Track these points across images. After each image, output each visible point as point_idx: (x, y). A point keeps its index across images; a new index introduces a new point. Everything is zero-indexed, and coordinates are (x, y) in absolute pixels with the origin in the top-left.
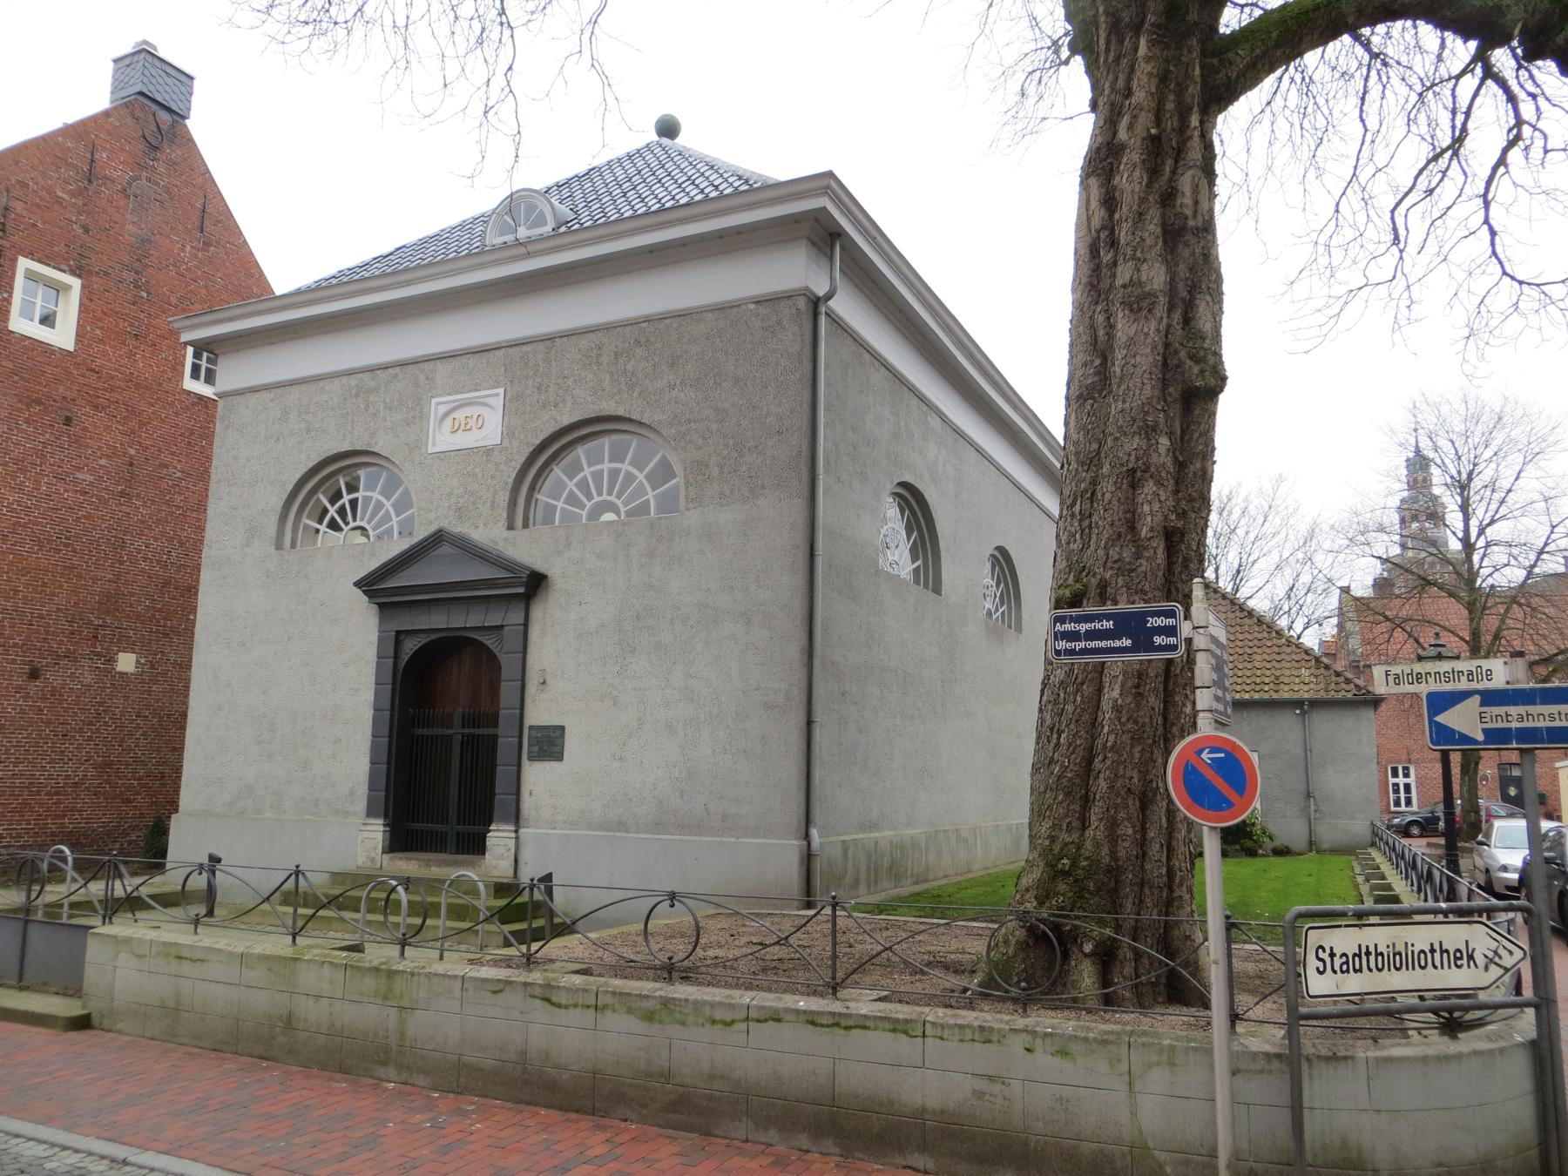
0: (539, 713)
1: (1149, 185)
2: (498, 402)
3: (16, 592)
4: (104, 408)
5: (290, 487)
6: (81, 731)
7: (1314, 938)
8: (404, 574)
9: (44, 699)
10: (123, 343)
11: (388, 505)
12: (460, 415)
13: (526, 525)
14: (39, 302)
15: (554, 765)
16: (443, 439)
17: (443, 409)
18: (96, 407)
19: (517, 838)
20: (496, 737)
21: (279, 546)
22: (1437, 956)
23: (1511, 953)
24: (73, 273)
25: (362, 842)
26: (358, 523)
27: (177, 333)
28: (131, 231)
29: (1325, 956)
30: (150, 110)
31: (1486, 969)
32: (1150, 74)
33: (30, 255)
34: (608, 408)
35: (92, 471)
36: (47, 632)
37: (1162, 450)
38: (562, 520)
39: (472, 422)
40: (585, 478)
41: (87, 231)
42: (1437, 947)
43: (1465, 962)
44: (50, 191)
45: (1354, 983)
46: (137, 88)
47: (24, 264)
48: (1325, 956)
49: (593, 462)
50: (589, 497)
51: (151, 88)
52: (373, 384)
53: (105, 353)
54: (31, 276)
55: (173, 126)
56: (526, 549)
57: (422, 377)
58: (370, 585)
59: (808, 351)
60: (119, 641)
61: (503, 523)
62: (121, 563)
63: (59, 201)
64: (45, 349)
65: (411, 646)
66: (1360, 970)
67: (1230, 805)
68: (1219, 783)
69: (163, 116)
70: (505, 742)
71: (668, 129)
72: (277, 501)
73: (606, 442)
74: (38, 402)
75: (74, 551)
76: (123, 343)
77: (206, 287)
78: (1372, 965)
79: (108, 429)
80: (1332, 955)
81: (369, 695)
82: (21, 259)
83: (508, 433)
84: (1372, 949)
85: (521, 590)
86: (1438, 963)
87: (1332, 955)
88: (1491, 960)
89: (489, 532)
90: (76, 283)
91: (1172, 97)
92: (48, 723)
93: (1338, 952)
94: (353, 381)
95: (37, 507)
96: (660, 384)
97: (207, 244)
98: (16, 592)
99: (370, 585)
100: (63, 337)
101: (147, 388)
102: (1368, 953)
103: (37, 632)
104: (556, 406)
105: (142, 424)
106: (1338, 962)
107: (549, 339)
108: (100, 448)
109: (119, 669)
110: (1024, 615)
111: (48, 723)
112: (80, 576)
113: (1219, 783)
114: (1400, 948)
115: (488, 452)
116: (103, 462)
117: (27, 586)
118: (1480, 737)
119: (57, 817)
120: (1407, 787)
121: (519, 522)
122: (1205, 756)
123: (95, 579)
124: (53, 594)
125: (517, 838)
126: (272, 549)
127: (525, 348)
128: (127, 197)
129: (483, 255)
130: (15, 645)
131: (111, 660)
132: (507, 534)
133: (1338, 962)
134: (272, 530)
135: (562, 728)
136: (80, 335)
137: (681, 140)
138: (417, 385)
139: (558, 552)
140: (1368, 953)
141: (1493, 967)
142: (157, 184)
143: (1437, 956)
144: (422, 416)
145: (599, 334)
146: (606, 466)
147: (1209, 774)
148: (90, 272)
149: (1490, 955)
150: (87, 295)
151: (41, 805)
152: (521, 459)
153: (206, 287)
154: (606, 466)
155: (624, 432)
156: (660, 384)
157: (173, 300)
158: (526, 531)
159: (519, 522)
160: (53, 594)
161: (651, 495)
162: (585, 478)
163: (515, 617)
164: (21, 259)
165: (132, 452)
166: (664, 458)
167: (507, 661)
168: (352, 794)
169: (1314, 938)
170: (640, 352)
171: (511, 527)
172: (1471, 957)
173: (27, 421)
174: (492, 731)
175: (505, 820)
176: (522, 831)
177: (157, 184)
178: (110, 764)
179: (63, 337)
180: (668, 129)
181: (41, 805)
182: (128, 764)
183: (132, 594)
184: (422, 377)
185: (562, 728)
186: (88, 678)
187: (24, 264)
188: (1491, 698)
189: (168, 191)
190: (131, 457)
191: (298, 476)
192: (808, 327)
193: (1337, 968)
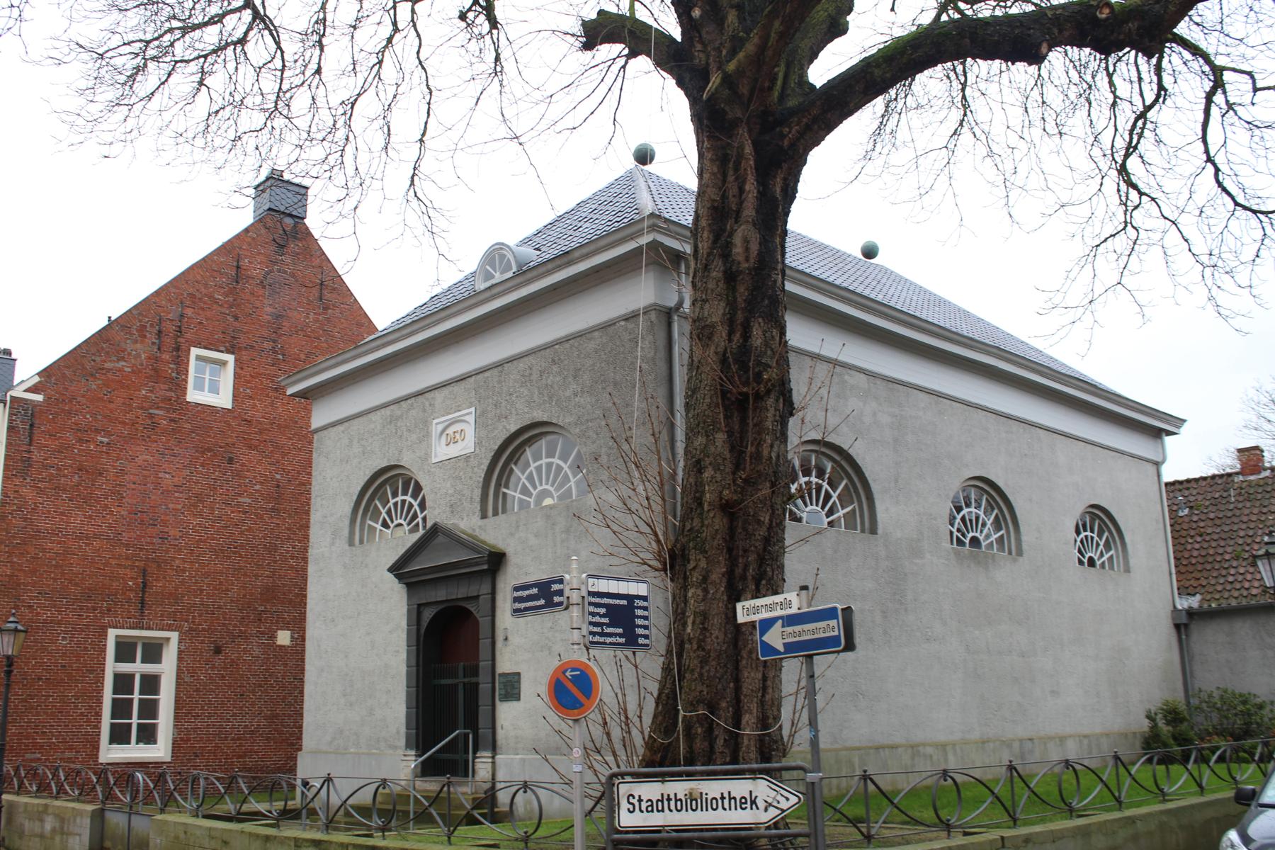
0: (505, 665)
1: (715, 242)
2: (471, 419)
3: (202, 591)
4: (256, 447)
5: (355, 498)
6: (253, 692)
7: (624, 789)
8: (418, 559)
9: (225, 668)
10: (267, 396)
12: (450, 431)
13: (495, 514)
14: (207, 377)
15: (515, 703)
16: (442, 451)
17: (440, 427)
18: (250, 448)
19: (493, 763)
20: (477, 684)
21: (351, 543)
22: (726, 802)
23: (787, 799)
24: (228, 352)
25: (401, 766)
26: (396, 522)
27: (284, 389)
28: (268, 310)
29: (635, 801)
30: (281, 220)
31: (766, 810)
32: (711, 160)
33: (199, 345)
34: (539, 415)
35: (250, 495)
36: (225, 619)
37: (719, 443)
38: (521, 508)
39: (458, 435)
41: (236, 318)
42: (726, 795)
43: (748, 805)
44: (211, 297)
45: (656, 820)
46: (266, 207)
47: (195, 352)
48: (635, 801)
49: (536, 461)
51: (277, 203)
52: (399, 413)
53: (254, 406)
54: (199, 358)
55: (295, 226)
56: (493, 533)
57: (427, 404)
58: (397, 569)
59: (662, 354)
60: (277, 622)
61: (478, 513)
62: (275, 562)
63: (216, 301)
64: (212, 410)
65: (428, 614)
66: (663, 810)
67: (582, 705)
68: (575, 691)
69: (288, 221)
70: (484, 687)
72: (347, 508)
73: (543, 443)
74: (209, 450)
75: (241, 556)
76: (267, 396)
77: (326, 341)
78: (673, 807)
79: (260, 463)
80: (640, 800)
81: (404, 656)
82: (192, 349)
83: (478, 443)
84: (672, 796)
85: (485, 567)
86: (726, 806)
87: (640, 800)
88: (770, 805)
89: (467, 522)
90: (230, 358)
91: (731, 172)
92: (230, 686)
93: (644, 798)
94: (387, 411)
95: (213, 527)
96: (568, 393)
97: (326, 308)
98: (202, 591)
99: (397, 569)
100: (223, 399)
101: (286, 427)
102: (669, 799)
103: (218, 619)
105: (284, 455)
106: (644, 805)
107: (499, 365)
108: (255, 477)
109: (279, 643)
110: (1024, 538)
111: (230, 686)
112: (245, 575)
113: (575, 691)
114: (696, 795)
115: (467, 458)
116: (258, 487)
117: (209, 585)
118: (782, 649)
119: (240, 757)
120: (151, 683)
121: (490, 512)
122: (568, 674)
123: (257, 576)
124: (228, 590)
125: (493, 763)
126: (346, 546)
127: (487, 374)
128: (264, 287)
129: (475, 298)
130: (204, 629)
131: (273, 637)
132: (481, 522)
133: (644, 805)
134: (346, 532)
135: (519, 674)
136: (235, 397)
138: (424, 411)
139: (512, 534)
140: (669, 799)
141: (771, 809)
142: (285, 272)
143: (726, 802)
144: (428, 435)
145: (531, 358)
146: (544, 461)
147: (570, 685)
148: (240, 349)
149: (770, 800)
150: (239, 364)
151: (229, 748)
152: (486, 462)
153: (326, 341)
156: (568, 393)
157: (303, 357)
158: (501, 517)
159: (490, 512)
160: (228, 590)
163: (485, 588)
164: (192, 349)
165: (278, 477)
166: (579, 452)
167: (484, 622)
168: (398, 732)
169: (624, 789)
170: (555, 369)
171: (484, 516)
172: (753, 802)
173: (203, 465)
174: (474, 680)
175: (485, 749)
176: (498, 757)
177: (285, 272)
178: (276, 716)
179: (223, 399)
181: (229, 748)
182: (290, 716)
183: (284, 585)
184: (427, 404)
185: (519, 674)
186: (257, 651)
187: (195, 352)
188: (791, 620)
189: (293, 275)
190: (278, 481)
192: (661, 335)
193: (644, 808)
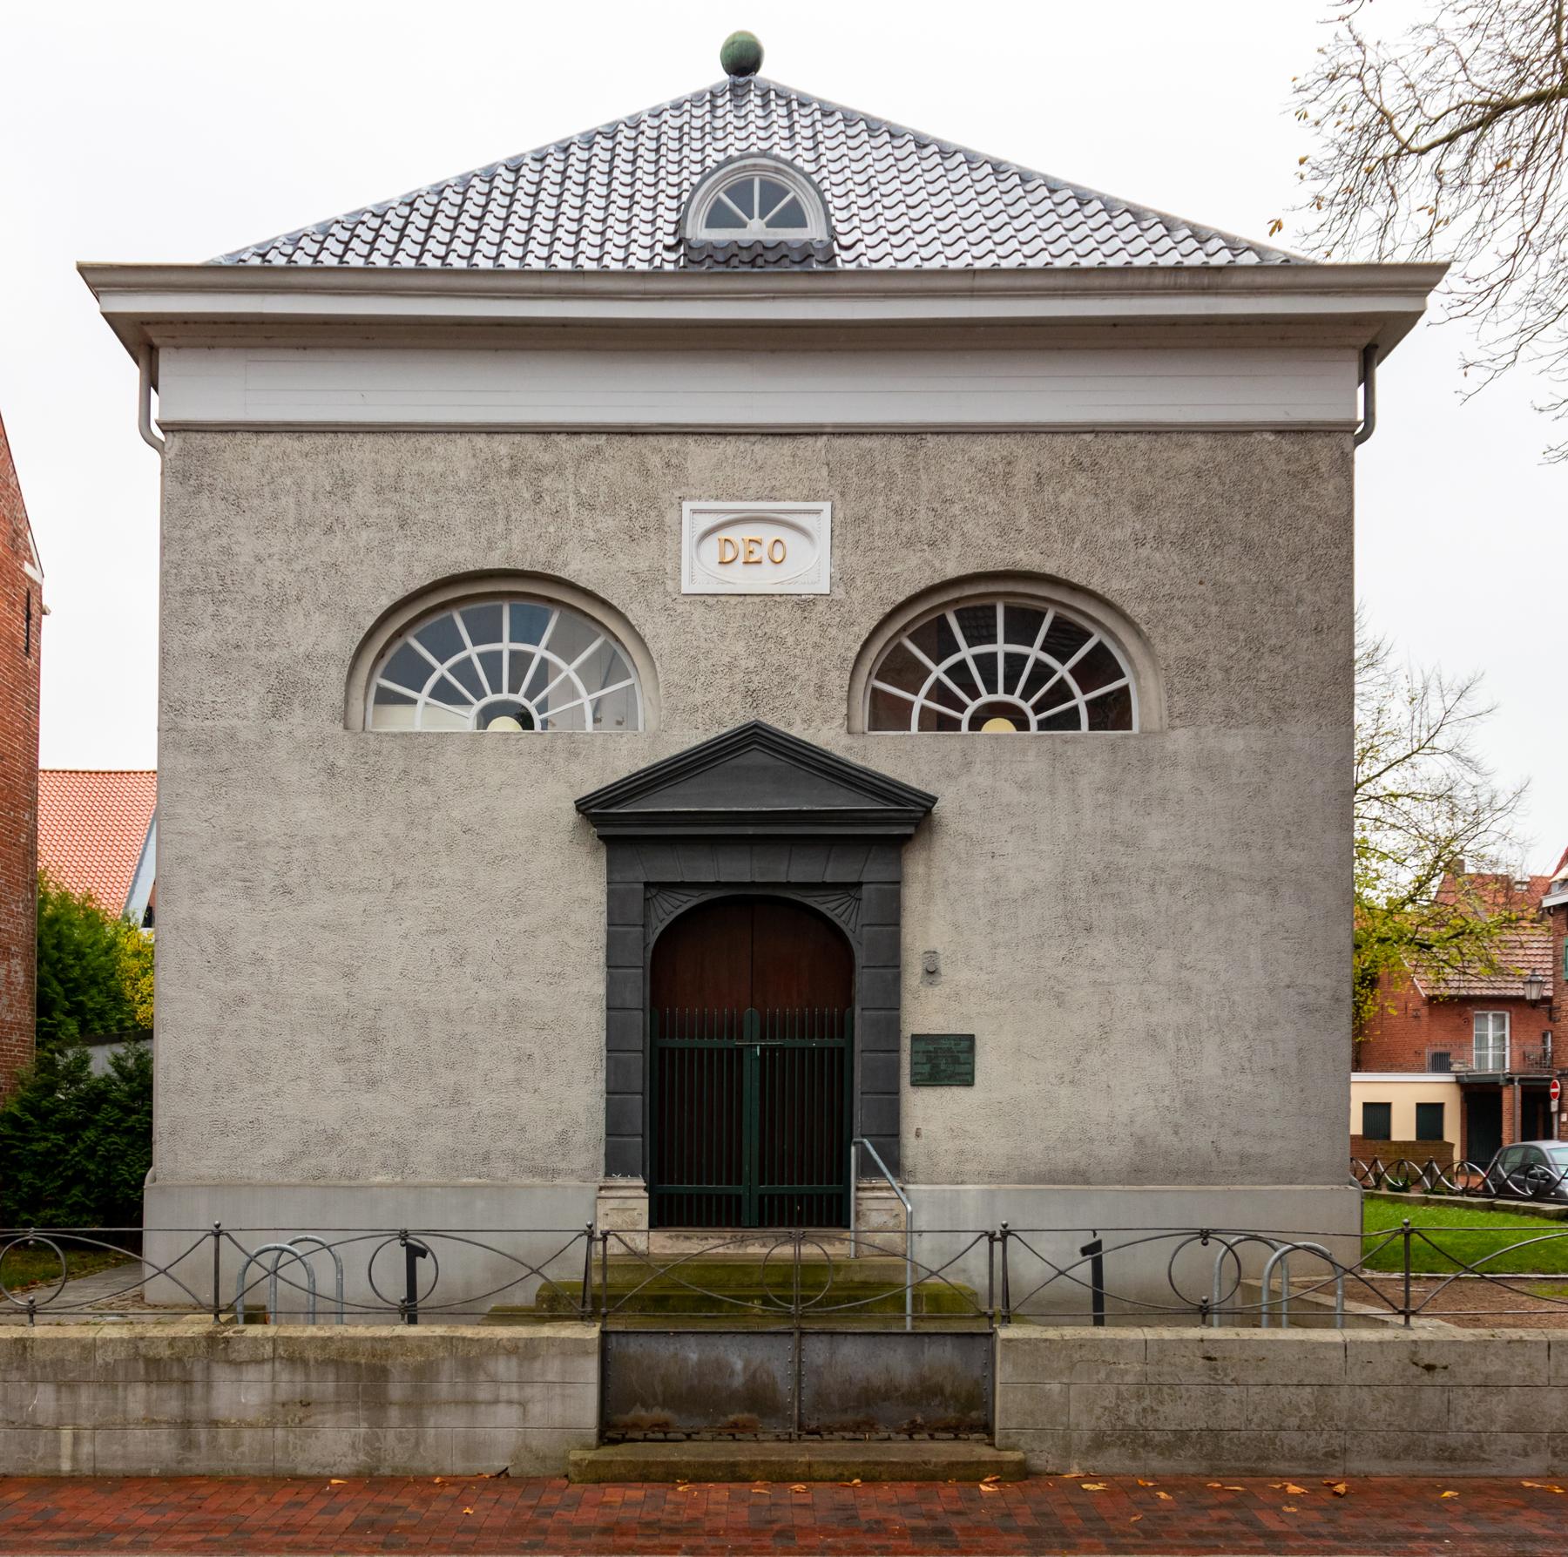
12: (738, 534)
104: (932, 544)
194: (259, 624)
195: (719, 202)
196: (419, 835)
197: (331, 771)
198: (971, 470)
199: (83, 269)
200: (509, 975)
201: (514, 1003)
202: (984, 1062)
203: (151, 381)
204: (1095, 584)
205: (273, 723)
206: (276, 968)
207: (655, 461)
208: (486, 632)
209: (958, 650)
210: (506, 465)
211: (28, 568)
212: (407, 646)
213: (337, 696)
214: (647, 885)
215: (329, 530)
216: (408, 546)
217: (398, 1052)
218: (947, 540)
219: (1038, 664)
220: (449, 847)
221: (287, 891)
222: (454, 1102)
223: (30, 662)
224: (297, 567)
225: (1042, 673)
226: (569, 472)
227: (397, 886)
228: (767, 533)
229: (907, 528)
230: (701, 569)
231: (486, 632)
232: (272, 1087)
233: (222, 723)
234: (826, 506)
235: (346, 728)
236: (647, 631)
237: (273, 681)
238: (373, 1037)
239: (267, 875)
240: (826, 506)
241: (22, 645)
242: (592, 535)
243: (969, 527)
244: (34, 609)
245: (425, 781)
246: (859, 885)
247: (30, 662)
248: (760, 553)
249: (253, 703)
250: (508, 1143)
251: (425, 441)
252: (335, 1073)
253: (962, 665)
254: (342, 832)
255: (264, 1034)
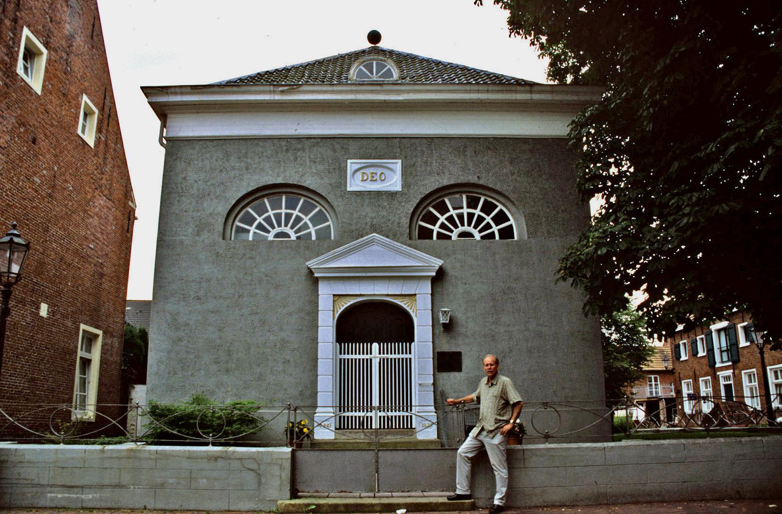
8: (344, 260)
11: (306, 219)
12: (368, 171)
15: (457, 374)
40: (292, 214)
50: (279, 225)
71: (374, 37)
104: (438, 174)
126: (221, 239)
135: (459, 354)
137: (382, 45)
154: (283, 211)
155: (293, 193)
161: (312, 230)
162: (292, 214)
180: (374, 37)
185: (459, 354)
191: (240, 195)
194: (194, 203)
195: (361, 69)
196: (249, 278)
197: (217, 255)
198: (451, 150)
199: (142, 88)
200: (281, 330)
201: (283, 340)
202: (466, 363)
203: (164, 125)
204: (498, 188)
205: (197, 238)
206: (194, 327)
207: (338, 147)
208: (276, 205)
209: (438, 219)
210: (285, 148)
211: (130, 203)
212: (248, 212)
213: (221, 228)
214: (334, 295)
215: (221, 171)
216: (249, 176)
217: (238, 359)
218: (444, 173)
219: (479, 216)
220: (260, 282)
221: (199, 298)
222: (259, 379)
223: (129, 235)
224: (209, 184)
225: (480, 219)
226: (307, 151)
227: (239, 296)
228: (379, 171)
229: (429, 168)
230: (355, 184)
231: (276, 205)
232: (190, 373)
233: (178, 238)
234: (400, 161)
235: (224, 239)
236: (335, 204)
237: (198, 223)
238: (229, 353)
239: (192, 293)
240: (400, 161)
241: (126, 228)
242: (315, 171)
243: (451, 168)
244: (132, 217)
245: (251, 258)
246: (415, 295)
247: (129, 235)
248: (377, 177)
249: (190, 231)
250: (280, 395)
251: (256, 142)
252: (214, 367)
253: (443, 224)
254: (220, 277)
255: (188, 352)
